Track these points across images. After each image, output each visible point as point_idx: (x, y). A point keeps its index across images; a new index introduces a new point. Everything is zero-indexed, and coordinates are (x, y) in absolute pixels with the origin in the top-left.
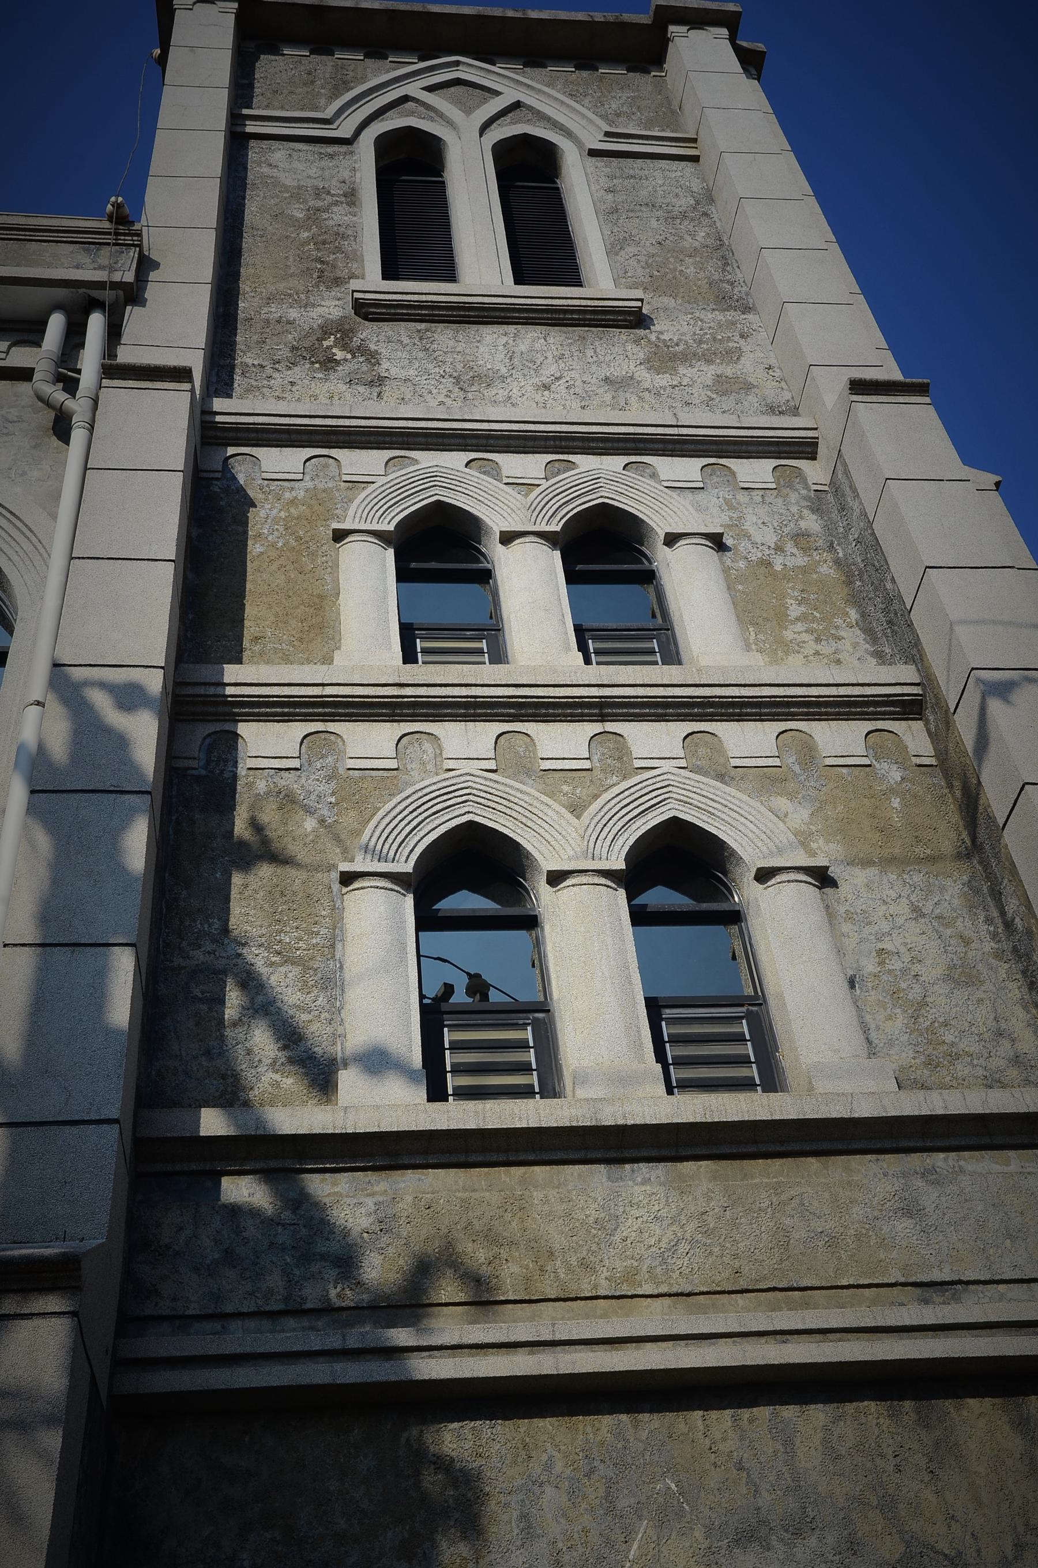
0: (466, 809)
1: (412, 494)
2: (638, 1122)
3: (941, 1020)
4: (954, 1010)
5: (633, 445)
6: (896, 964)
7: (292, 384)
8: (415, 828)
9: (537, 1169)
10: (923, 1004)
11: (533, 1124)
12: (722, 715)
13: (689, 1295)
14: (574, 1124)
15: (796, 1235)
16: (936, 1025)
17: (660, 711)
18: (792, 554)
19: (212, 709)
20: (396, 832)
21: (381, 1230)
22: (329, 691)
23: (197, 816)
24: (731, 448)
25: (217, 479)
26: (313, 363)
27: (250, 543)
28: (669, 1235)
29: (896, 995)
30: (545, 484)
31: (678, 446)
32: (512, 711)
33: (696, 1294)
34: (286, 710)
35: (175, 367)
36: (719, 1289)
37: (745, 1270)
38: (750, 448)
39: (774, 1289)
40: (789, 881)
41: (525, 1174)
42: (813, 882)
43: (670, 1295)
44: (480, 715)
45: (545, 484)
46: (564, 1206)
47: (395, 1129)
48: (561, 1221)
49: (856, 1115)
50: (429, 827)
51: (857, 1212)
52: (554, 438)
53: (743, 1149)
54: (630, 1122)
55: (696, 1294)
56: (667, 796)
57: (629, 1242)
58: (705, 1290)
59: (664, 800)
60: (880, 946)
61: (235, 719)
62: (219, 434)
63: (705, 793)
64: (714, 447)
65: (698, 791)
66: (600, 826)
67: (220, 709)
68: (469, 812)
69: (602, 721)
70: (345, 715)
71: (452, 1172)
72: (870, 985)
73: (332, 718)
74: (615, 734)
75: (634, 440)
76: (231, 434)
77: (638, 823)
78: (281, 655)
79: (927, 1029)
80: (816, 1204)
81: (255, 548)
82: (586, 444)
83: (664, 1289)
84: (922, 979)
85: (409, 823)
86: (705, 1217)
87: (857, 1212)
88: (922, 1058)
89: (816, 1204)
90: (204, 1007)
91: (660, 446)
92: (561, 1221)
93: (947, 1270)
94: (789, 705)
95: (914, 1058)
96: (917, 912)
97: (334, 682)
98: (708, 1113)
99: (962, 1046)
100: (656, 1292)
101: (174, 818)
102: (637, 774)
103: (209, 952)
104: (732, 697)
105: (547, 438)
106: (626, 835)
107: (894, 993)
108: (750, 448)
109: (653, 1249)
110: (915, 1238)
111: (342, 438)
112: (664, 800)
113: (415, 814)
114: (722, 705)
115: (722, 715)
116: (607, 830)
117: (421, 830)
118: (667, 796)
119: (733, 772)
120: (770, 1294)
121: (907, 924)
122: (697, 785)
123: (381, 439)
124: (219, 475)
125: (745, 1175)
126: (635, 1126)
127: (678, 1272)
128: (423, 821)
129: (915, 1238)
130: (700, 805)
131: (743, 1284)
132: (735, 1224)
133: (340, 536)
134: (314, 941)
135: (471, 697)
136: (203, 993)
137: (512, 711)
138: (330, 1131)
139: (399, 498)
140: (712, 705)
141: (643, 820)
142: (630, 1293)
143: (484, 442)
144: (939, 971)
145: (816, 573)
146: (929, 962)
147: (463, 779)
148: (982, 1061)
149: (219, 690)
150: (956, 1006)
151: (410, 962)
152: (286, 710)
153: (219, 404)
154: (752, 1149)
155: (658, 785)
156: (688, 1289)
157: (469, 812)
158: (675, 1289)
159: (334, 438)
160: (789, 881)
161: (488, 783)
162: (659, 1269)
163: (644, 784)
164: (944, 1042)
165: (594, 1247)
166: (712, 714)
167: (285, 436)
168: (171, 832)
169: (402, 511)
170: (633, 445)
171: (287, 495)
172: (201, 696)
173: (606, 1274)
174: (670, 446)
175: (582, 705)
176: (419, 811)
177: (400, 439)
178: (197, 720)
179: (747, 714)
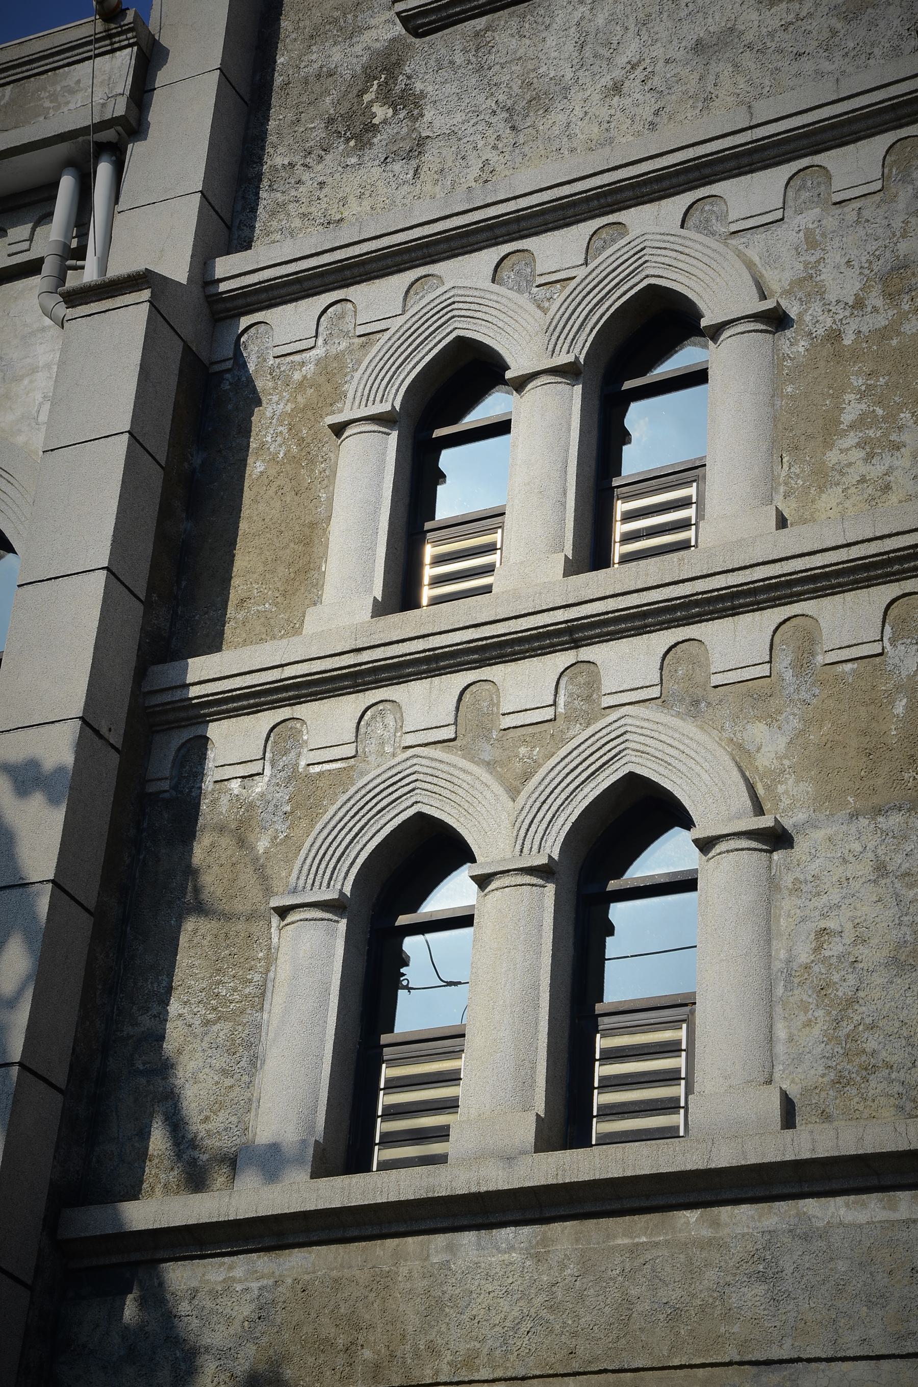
0: (413, 800)
1: (426, 339)
2: (490, 1189)
3: (868, 1021)
4: (887, 1006)
5: (696, 174)
6: (834, 948)
7: (322, 184)
8: (357, 835)
9: (410, 1240)
10: (852, 1001)
11: (393, 1198)
12: (712, 612)
13: (524, 1378)
14: (430, 1195)
15: (639, 1308)
16: (861, 1028)
17: (637, 623)
18: (875, 310)
19: (183, 715)
20: (335, 844)
21: (259, 1318)
22: (289, 672)
23: (163, 851)
24: (828, 135)
25: (228, 371)
26: (348, 140)
27: (250, 460)
28: (515, 1313)
29: (823, 992)
30: (582, 272)
31: (756, 157)
32: (476, 656)
33: (530, 1378)
34: (252, 701)
35: (129, 276)
36: (551, 1372)
37: (580, 1351)
38: (854, 127)
39: (605, 1371)
40: (728, 851)
41: (398, 1246)
42: (765, 847)
43: (506, 1380)
44: (444, 668)
45: (582, 272)
46: (425, 1282)
47: (270, 1213)
48: (419, 1300)
49: (713, 1166)
50: (374, 830)
51: (711, 1275)
52: (597, 196)
53: (607, 1207)
54: (483, 1189)
55: (530, 1378)
56: (622, 746)
57: (476, 1321)
58: (538, 1373)
59: (620, 752)
60: (822, 924)
61: (204, 721)
62: (229, 305)
63: (663, 738)
64: (805, 142)
65: (656, 735)
66: (538, 804)
67: (191, 713)
68: (416, 802)
69: (577, 647)
70: (311, 694)
71: (333, 1247)
72: (796, 980)
73: (297, 700)
74: (589, 662)
75: (697, 167)
76: (240, 302)
77: (587, 790)
78: (262, 620)
79: (848, 1036)
80: (668, 1269)
81: (256, 467)
82: (638, 192)
83: (499, 1373)
84: (860, 965)
85: (351, 830)
86: (554, 1289)
87: (711, 1275)
88: (832, 1075)
89: (668, 1269)
90: (143, 1081)
91: (732, 164)
92: (419, 1300)
93: (788, 1343)
94: (790, 584)
95: (823, 1076)
96: (881, 869)
97: (292, 661)
98: (560, 1173)
99: (884, 1054)
100: (491, 1377)
101: (141, 857)
102: (604, 716)
103: (155, 1016)
104: (718, 590)
105: (588, 200)
106: (570, 808)
107: (822, 990)
108: (854, 127)
109: (497, 1329)
110: (762, 1308)
111: (356, 271)
112: (620, 752)
113: (357, 818)
114: (709, 601)
115: (712, 612)
116: (546, 807)
117: (364, 835)
118: (622, 746)
119: (714, 696)
120: (603, 1376)
121: (862, 890)
122: (655, 727)
123: (398, 259)
124: (229, 365)
125: (608, 1236)
126: (488, 1193)
127: (516, 1354)
128: (366, 824)
129: (762, 1308)
130: (657, 754)
131: (575, 1366)
132: (581, 1297)
133: (339, 430)
134: (247, 991)
135: (429, 650)
136: (144, 1064)
137: (476, 656)
138: (215, 1220)
139: (410, 350)
140: (697, 603)
141: (592, 785)
142: (466, 1379)
143: (514, 227)
144: (880, 956)
145: (899, 333)
146: (874, 942)
147: (409, 763)
148: (902, 1075)
149: (178, 695)
150: (892, 1000)
151: (331, 1004)
152: (252, 701)
153: (224, 266)
154: (616, 1206)
155: (613, 735)
156: (522, 1372)
157: (416, 802)
158: (509, 1374)
159: (348, 273)
160: (728, 851)
161: (434, 764)
162: (499, 1351)
163: (597, 736)
164: (864, 1051)
165: (444, 1329)
166: (699, 615)
167: (296, 288)
168: (137, 875)
169: (414, 367)
170: (696, 174)
171: (297, 376)
172: (168, 703)
173: (449, 1358)
174: (745, 160)
175: (549, 635)
176: (361, 814)
177: (420, 253)
178: (173, 728)
179: (741, 606)
